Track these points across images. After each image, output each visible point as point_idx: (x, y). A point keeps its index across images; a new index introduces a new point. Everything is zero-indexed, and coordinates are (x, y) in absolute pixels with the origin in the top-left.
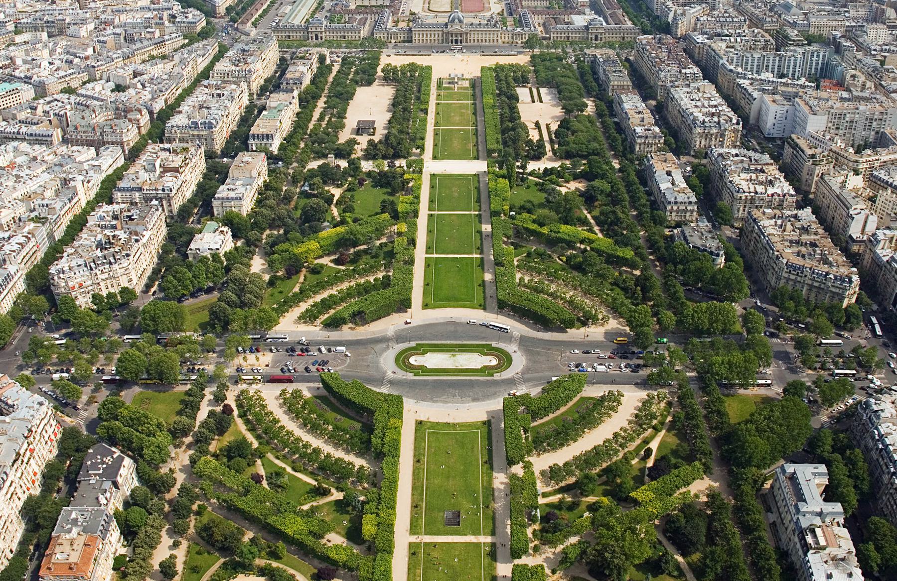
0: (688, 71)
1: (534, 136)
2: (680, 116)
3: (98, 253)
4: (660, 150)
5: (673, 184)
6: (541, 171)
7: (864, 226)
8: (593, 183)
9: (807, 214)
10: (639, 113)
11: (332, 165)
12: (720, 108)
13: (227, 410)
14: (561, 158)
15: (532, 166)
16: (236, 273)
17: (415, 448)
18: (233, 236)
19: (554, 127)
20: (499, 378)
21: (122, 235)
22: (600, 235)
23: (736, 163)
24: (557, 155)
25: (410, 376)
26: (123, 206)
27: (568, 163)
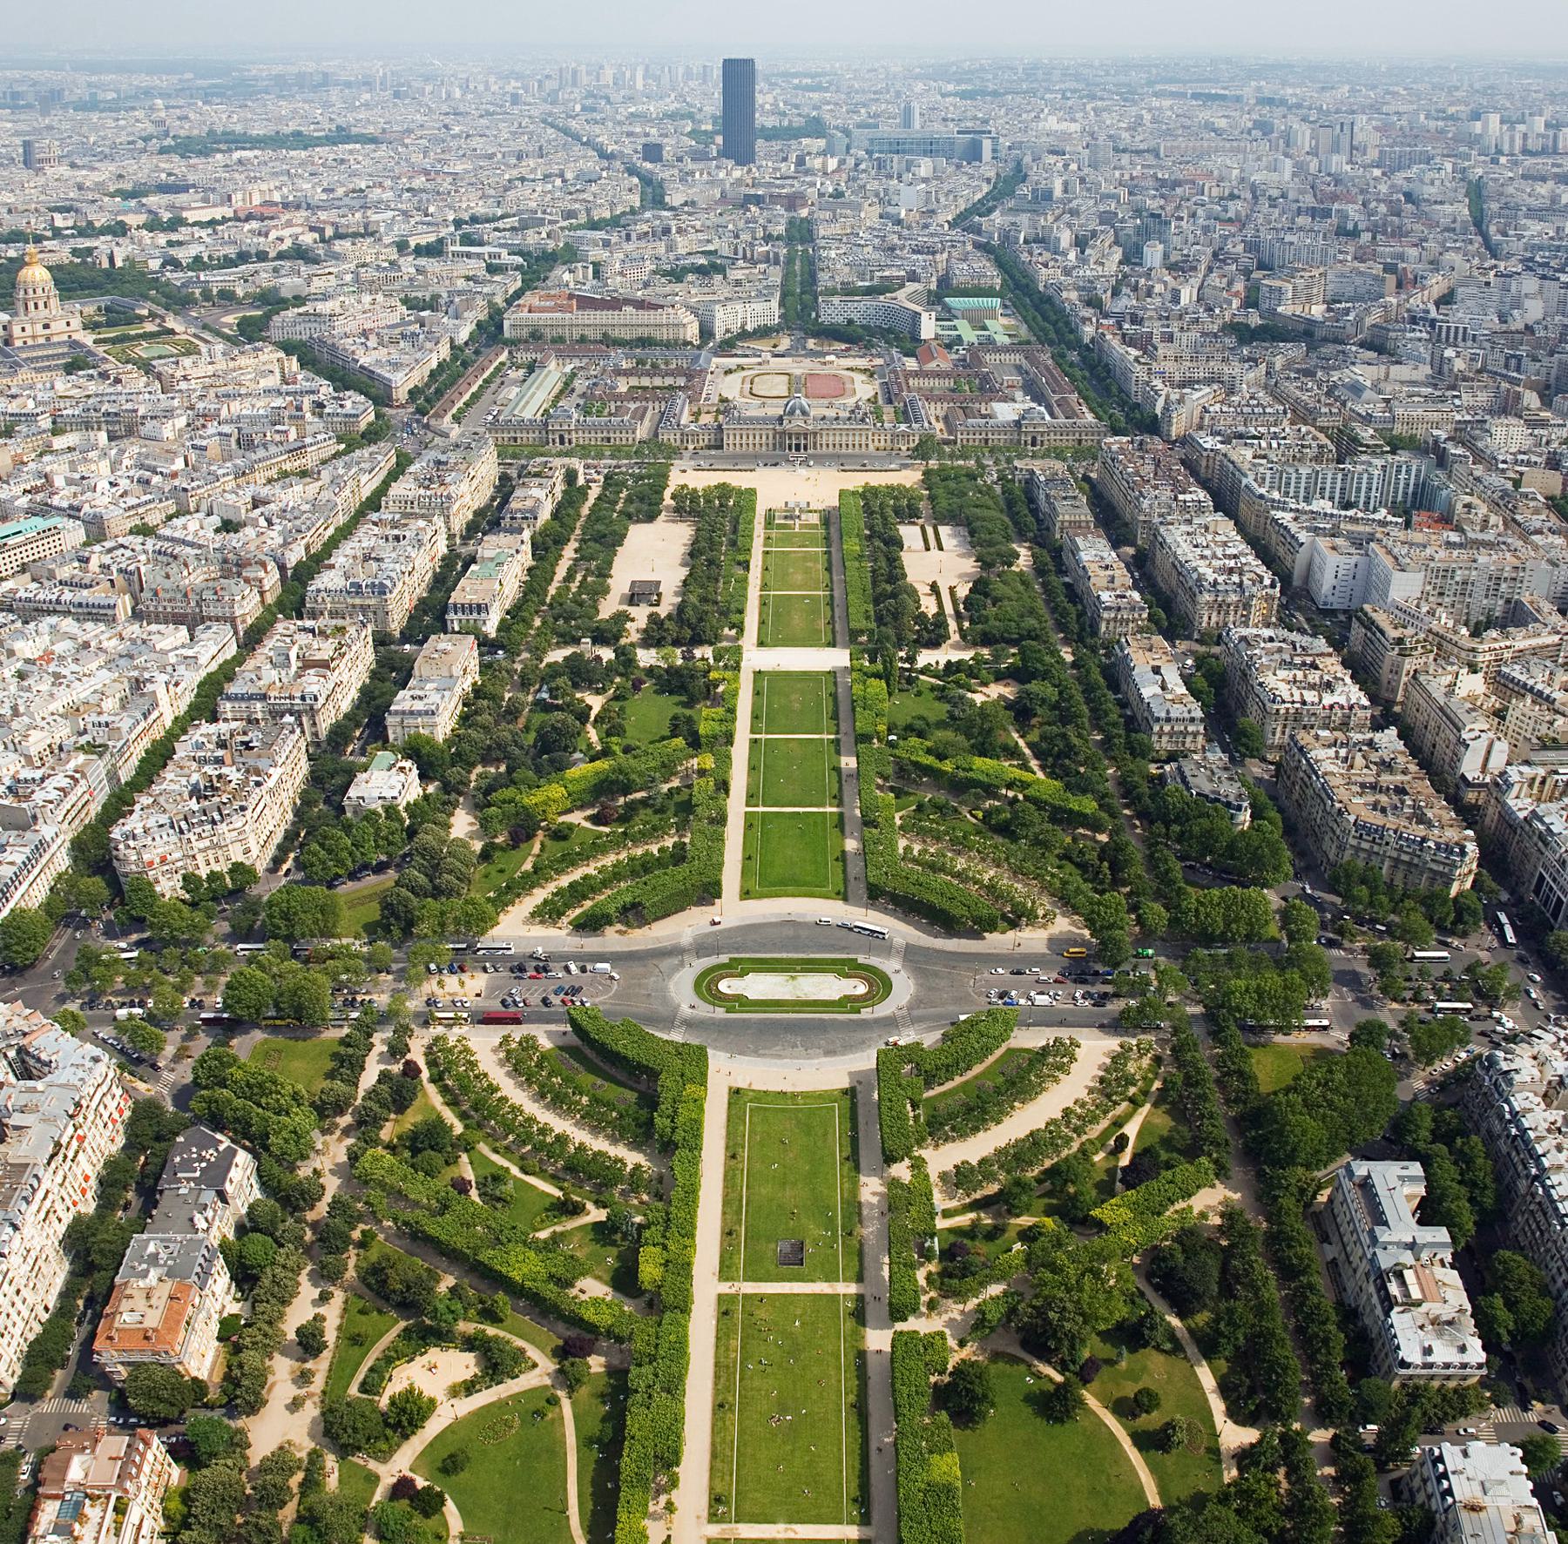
0: (1188, 497)
1: (929, 606)
3: (194, 805)
4: (1141, 630)
5: (1164, 688)
7: (1486, 760)
9: (1389, 739)
13: (411, 1070)
14: (975, 644)
15: (925, 658)
18: (421, 777)
19: (963, 591)
21: (234, 774)
22: (1040, 775)
23: (1269, 653)
24: (967, 640)
25: (720, 1013)
26: (234, 725)
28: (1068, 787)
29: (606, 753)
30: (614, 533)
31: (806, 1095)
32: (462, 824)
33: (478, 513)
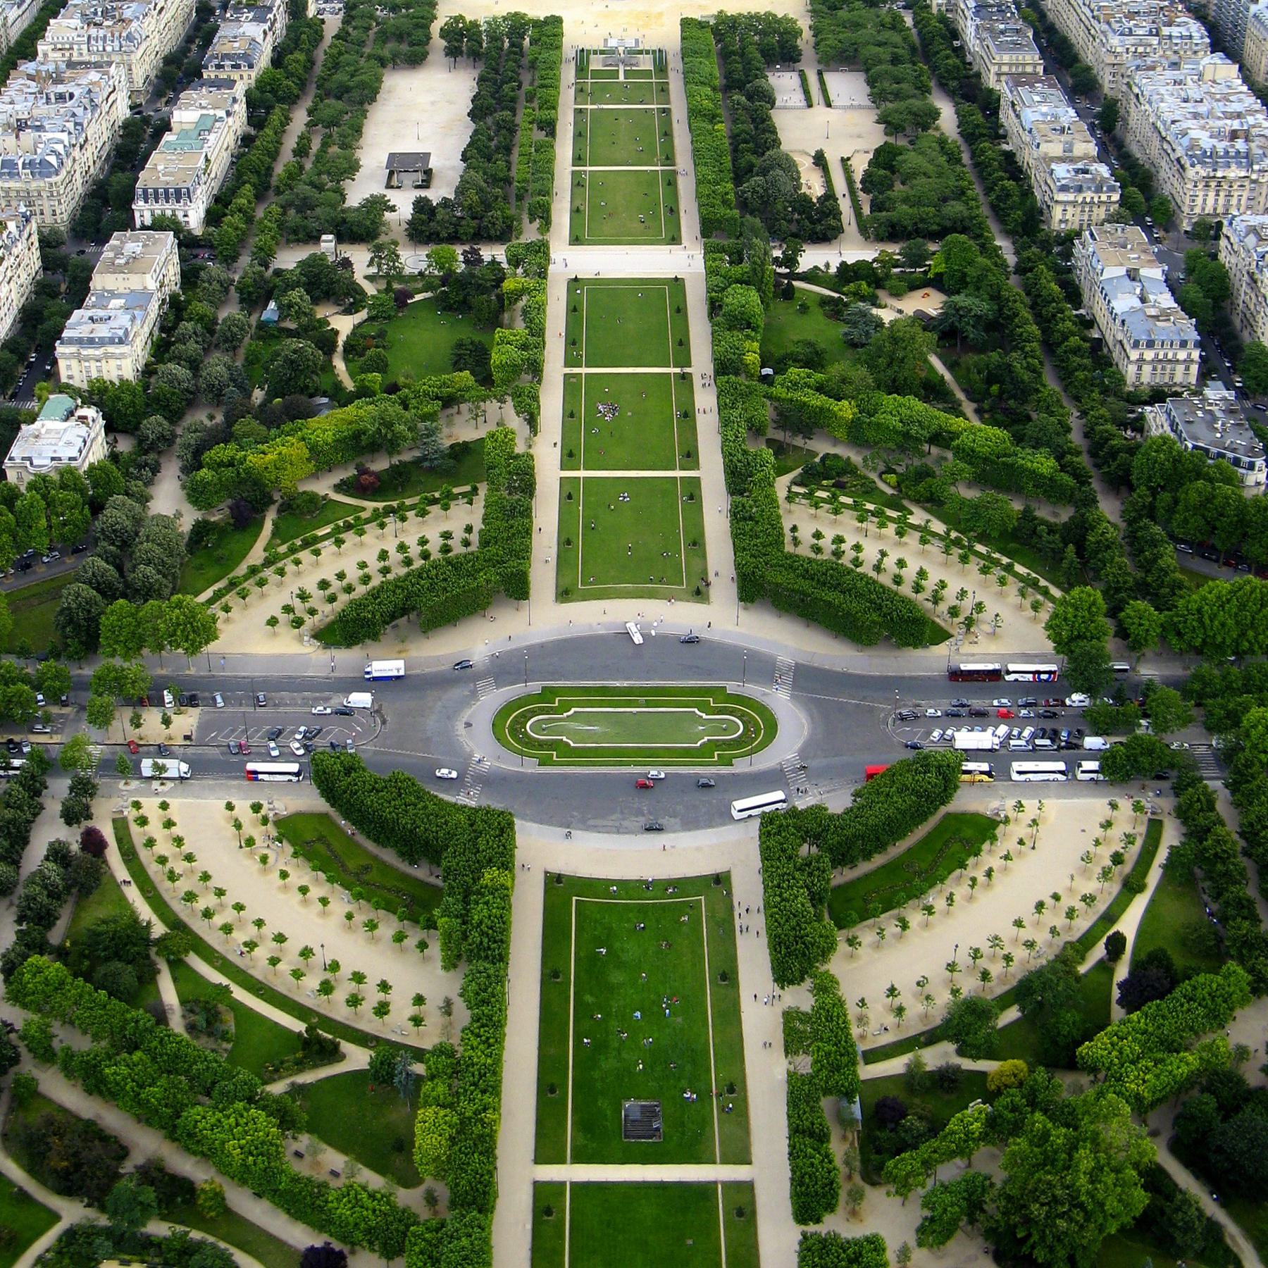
0: (1175, 31)
1: (813, 185)
2: (1156, 142)
4: (1111, 219)
5: (1143, 300)
6: (833, 270)
8: (956, 298)
10: (1062, 130)
11: (331, 259)
12: (1251, 120)
13: (93, 843)
14: (880, 239)
15: (812, 258)
16: (117, 512)
17: (641, 597)
18: (109, 429)
19: (860, 166)
20: (747, 769)
22: (977, 423)
24: (869, 231)
25: (530, 767)
27: (893, 249)
28: (1019, 439)
29: (363, 392)
30: (363, 86)
31: (625, 885)
32: (168, 499)
33: (170, 60)
